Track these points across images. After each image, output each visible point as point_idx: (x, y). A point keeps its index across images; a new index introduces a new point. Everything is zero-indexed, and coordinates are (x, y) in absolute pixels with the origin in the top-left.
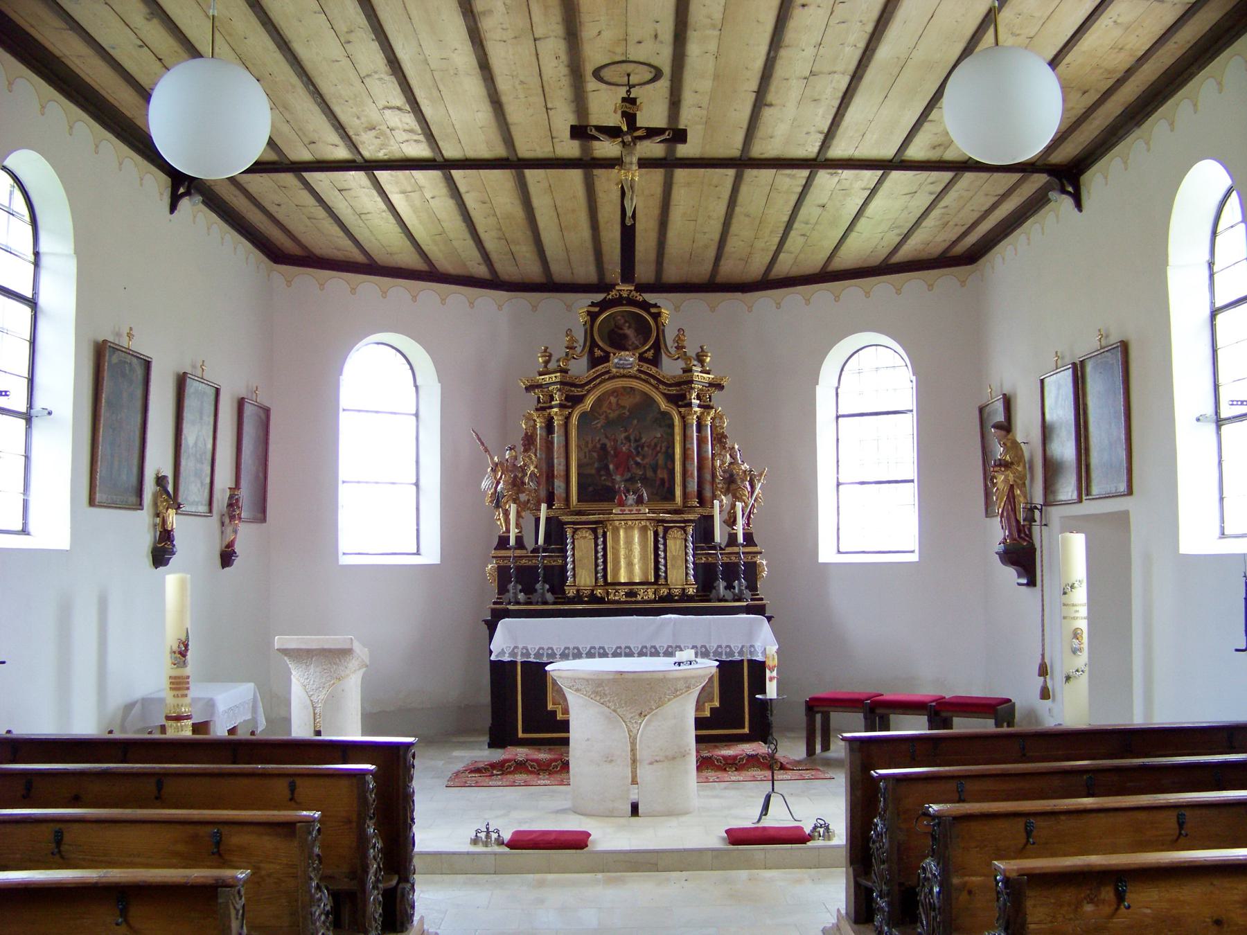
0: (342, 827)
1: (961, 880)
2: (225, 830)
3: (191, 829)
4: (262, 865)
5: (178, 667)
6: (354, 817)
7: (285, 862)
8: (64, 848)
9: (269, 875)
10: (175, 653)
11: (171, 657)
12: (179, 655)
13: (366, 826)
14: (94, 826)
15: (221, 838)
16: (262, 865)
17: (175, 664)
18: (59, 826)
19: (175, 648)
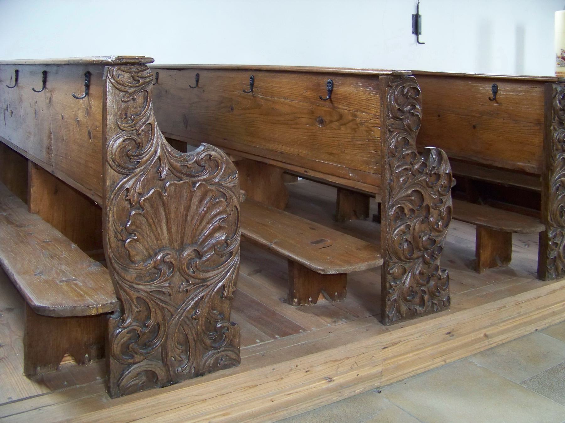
0: (533, 128)
1: (440, 359)
2: (337, 81)
3: (315, 79)
4: (358, 113)
5: (561, 66)
6: (542, 119)
7: (374, 113)
8: (255, 89)
9: (362, 123)
10: (559, 57)
11: (557, 60)
12: (562, 59)
13: (552, 128)
14: (267, 74)
15: (332, 87)
16: (358, 113)
17: (559, 65)
18: (254, 74)
19: (559, 55)
